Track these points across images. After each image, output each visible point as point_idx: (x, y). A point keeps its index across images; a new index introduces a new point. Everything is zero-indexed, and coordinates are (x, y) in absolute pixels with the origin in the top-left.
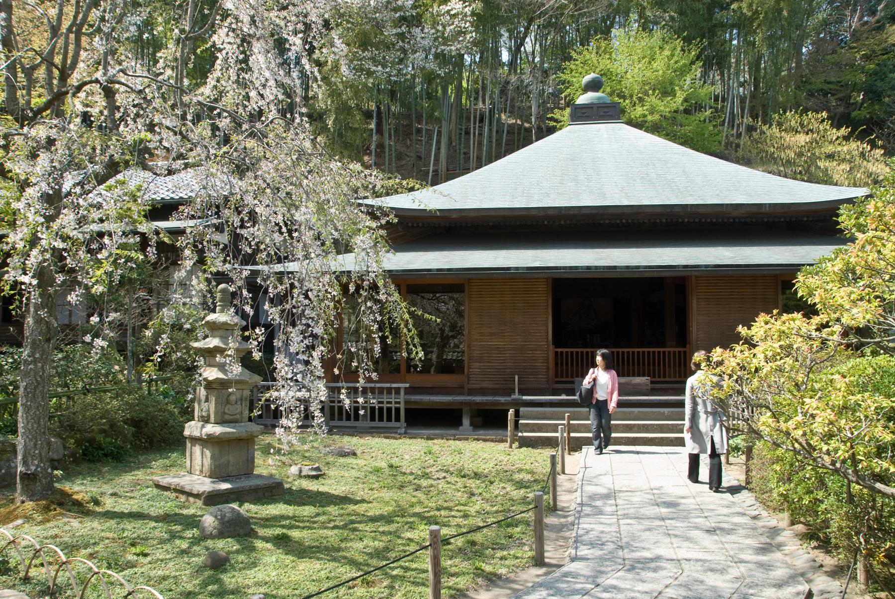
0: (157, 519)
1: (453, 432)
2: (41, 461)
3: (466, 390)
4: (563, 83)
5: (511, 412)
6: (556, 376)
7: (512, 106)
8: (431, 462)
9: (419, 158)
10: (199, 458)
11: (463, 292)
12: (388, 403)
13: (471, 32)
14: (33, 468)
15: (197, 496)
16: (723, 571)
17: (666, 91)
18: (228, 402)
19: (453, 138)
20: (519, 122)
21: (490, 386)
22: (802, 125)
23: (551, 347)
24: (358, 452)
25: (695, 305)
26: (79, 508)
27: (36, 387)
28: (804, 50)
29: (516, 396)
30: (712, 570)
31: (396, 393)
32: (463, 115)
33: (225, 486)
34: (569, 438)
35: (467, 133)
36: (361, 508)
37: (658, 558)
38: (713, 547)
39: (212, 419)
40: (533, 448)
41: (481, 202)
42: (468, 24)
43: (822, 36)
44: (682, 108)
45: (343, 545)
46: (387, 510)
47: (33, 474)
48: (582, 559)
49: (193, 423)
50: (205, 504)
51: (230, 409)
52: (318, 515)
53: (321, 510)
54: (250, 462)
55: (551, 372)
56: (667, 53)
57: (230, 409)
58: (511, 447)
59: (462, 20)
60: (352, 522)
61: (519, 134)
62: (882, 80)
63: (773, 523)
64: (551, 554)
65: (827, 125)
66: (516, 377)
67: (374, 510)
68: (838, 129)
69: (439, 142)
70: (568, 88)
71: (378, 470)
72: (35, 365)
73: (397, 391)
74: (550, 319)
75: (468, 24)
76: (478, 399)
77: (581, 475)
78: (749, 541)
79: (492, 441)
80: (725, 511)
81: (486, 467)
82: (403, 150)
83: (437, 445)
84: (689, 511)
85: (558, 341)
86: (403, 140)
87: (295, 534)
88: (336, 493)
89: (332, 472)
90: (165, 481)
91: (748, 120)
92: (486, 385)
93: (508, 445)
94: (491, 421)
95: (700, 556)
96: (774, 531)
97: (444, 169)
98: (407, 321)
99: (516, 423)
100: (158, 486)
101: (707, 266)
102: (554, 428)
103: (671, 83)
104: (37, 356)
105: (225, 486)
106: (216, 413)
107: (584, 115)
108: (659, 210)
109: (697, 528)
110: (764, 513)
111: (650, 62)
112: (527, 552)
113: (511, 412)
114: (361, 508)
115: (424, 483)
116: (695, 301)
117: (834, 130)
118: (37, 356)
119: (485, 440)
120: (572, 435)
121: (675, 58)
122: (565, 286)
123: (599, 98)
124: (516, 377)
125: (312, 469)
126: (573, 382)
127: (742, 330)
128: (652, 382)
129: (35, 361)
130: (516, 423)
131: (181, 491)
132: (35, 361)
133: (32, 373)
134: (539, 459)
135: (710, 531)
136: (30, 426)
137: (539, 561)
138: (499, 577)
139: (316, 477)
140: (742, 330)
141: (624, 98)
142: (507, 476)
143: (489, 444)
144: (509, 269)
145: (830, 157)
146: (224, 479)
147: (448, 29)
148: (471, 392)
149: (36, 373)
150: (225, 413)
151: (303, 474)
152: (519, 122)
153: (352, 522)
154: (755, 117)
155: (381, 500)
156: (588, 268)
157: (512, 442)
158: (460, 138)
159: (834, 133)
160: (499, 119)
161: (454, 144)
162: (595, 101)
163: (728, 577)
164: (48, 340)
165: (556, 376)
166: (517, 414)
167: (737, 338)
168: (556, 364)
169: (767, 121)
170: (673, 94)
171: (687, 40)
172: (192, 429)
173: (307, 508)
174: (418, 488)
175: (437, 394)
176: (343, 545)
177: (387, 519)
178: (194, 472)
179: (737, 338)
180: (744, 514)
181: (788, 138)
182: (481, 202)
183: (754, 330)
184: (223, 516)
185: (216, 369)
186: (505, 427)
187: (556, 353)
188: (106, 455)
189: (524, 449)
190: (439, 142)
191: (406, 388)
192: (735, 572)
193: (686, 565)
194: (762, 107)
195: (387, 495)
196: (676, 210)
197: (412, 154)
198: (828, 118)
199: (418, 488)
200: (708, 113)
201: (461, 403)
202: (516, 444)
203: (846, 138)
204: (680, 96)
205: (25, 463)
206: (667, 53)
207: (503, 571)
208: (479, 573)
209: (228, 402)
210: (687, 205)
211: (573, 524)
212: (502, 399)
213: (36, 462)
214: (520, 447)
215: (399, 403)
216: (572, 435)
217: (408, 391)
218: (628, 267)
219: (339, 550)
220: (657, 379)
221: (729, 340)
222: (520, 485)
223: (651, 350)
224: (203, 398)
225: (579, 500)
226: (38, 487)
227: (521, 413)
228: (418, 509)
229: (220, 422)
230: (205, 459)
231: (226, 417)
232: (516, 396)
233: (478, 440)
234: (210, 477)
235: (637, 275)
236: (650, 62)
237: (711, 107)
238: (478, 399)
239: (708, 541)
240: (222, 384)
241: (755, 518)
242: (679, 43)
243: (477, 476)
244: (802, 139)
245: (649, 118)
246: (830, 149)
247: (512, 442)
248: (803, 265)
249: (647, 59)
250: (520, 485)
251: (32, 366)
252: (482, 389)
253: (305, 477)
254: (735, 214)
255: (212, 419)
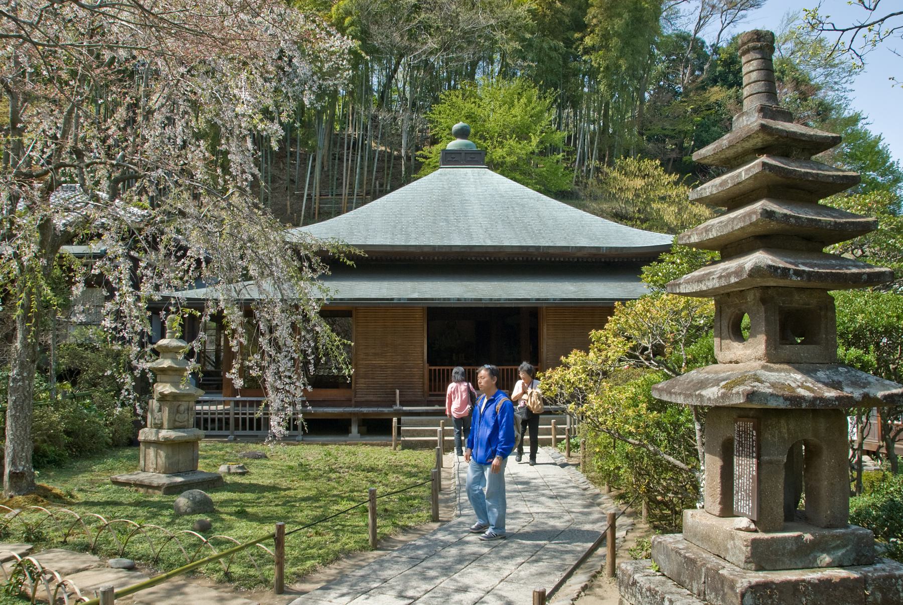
0: (130, 504)
1: (342, 438)
2: (27, 462)
3: (353, 402)
4: (431, 122)
5: (395, 420)
6: (430, 390)
7: (383, 135)
8: (333, 460)
9: (292, 181)
10: (153, 458)
11: (351, 316)
13: (348, 70)
14: (21, 468)
15: (158, 488)
16: (560, 517)
17: (522, 134)
18: (178, 412)
19: (325, 163)
20: (389, 150)
21: (374, 399)
22: (639, 170)
23: (426, 365)
24: (268, 454)
25: (545, 330)
26: (58, 499)
27: (24, 401)
28: (646, 95)
29: (397, 407)
30: (553, 517)
32: (336, 141)
33: (179, 479)
34: (444, 441)
35: (341, 159)
36: (292, 493)
37: (517, 512)
38: (554, 506)
39: (166, 425)
40: (414, 449)
42: (345, 62)
43: (662, 83)
44: (537, 151)
45: (290, 515)
46: (313, 493)
47: (21, 473)
48: (465, 515)
49: (146, 429)
50: (165, 493)
51: (180, 417)
52: (259, 498)
53: (260, 495)
54: (195, 460)
55: (426, 387)
56: (523, 100)
57: (180, 417)
58: (395, 449)
59: (340, 56)
60: (289, 502)
61: (389, 161)
62: (707, 132)
63: (597, 491)
64: (443, 513)
65: (660, 170)
66: (398, 391)
67: (302, 494)
68: (670, 174)
69: (313, 167)
70: (435, 127)
71: (291, 468)
72: (24, 382)
75: (345, 62)
76: (365, 410)
77: (456, 467)
78: (580, 502)
79: (378, 445)
80: (565, 485)
81: (381, 463)
82: (277, 172)
83: (332, 448)
84: (538, 487)
85: (431, 361)
86: (276, 163)
87: (249, 510)
88: (265, 484)
89: (252, 470)
90: (123, 477)
91: (594, 163)
92: (371, 398)
93: (392, 448)
94: (377, 428)
95: (546, 511)
96: (597, 496)
97: (318, 194)
99: (399, 428)
100: (115, 482)
101: (554, 299)
102: (434, 433)
103: (529, 127)
104: (25, 374)
105: (179, 479)
106: (169, 420)
107: (452, 159)
108: (517, 250)
109: (543, 495)
110: (592, 487)
111: (510, 108)
112: (425, 514)
113: (395, 420)
114: (292, 493)
115: (333, 476)
116: (545, 327)
117: (667, 176)
118: (25, 374)
119: (372, 445)
120: (446, 438)
121: (533, 105)
122: (439, 314)
123: (467, 145)
124: (398, 391)
125: (239, 468)
127: (563, 358)
129: (23, 379)
130: (399, 428)
131: (141, 485)
132: (23, 379)
133: (21, 389)
134: (424, 458)
135: (551, 498)
136: (18, 433)
137: (435, 518)
138: (410, 528)
139: (243, 474)
140: (563, 358)
141: (485, 139)
142: (396, 469)
143: (376, 448)
144: (392, 299)
145: (663, 199)
146: (178, 474)
147: (326, 66)
148: (359, 404)
149: (24, 389)
150: (175, 421)
151: (232, 471)
152: (389, 150)
153: (289, 502)
154: (601, 159)
155: (304, 488)
156: (459, 299)
157: (396, 446)
158: (333, 165)
159: (667, 179)
160: (370, 147)
161: (326, 169)
162: (464, 148)
163: (562, 520)
164: (33, 362)
166: (399, 421)
167: (560, 363)
168: (430, 380)
169: (611, 164)
170: (529, 139)
171: (543, 90)
172: (145, 434)
173: (247, 494)
174: (329, 479)
175: (328, 406)
176: (290, 515)
177: (315, 499)
178: (151, 468)
179: (560, 363)
180: (577, 487)
181: (627, 182)
182: (366, 238)
183: (570, 358)
184: (194, 498)
185: (169, 385)
186: (391, 434)
187: (430, 370)
188: (48, 462)
189: (405, 451)
190: (313, 167)
192: (567, 517)
193: (534, 515)
194: (609, 149)
195: (308, 484)
196: (531, 250)
197: (285, 177)
198: (661, 165)
199: (329, 479)
200: (560, 156)
201: (351, 413)
202: (400, 447)
203: (676, 183)
204: (535, 141)
205: (13, 463)
206: (523, 100)
207: (412, 524)
208: (395, 525)
209: (178, 412)
210: (540, 247)
211: (456, 497)
212: (386, 410)
213: (23, 463)
214: (403, 449)
216: (446, 438)
218: (491, 299)
219: (288, 518)
221: (556, 363)
222: (410, 475)
223: (509, 367)
224: (156, 409)
225: (457, 483)
226: (24, 484)
227: (402, 421)
228: (335, 492)
229: (173, 428)
230: (159, 459)
231: (177, 424)
232: (397, 407)
233: (366, 444)
234: (164, 473)
235: (498, 306)
236: (510, 108)
237: (564, 151)
238: (365, 410)
239: (550, 503)
240: (174, 397)
241: (585, 489)
242: (535, 92)
243: (372, 469)
244: (639, 183)
245: (508, 159)
246: (662, 192)
247: (396, 446)
248: (630, 300)
249: (506, 106)
250: (410, 475)
251: (20, 383)
252: (367, 401)
253: (234, 474)
254: (579, 254)
255: (166, 425)
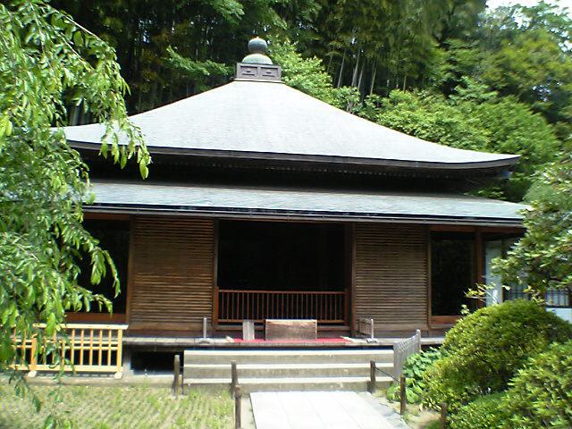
5: (177, 357)
12: (95, 345)
25: (354, 252)
31: (113, 335)
41: (432, 211)
73: (115, 332)
74: (216, 261)
98: (87, 255)
126: (241, 324)
128: (318, 324)
165: (220, 318)
182: (195, 141)
191: (124, 331)
215: (116, 346)
217: (125, 333)
220: (323, 321)
